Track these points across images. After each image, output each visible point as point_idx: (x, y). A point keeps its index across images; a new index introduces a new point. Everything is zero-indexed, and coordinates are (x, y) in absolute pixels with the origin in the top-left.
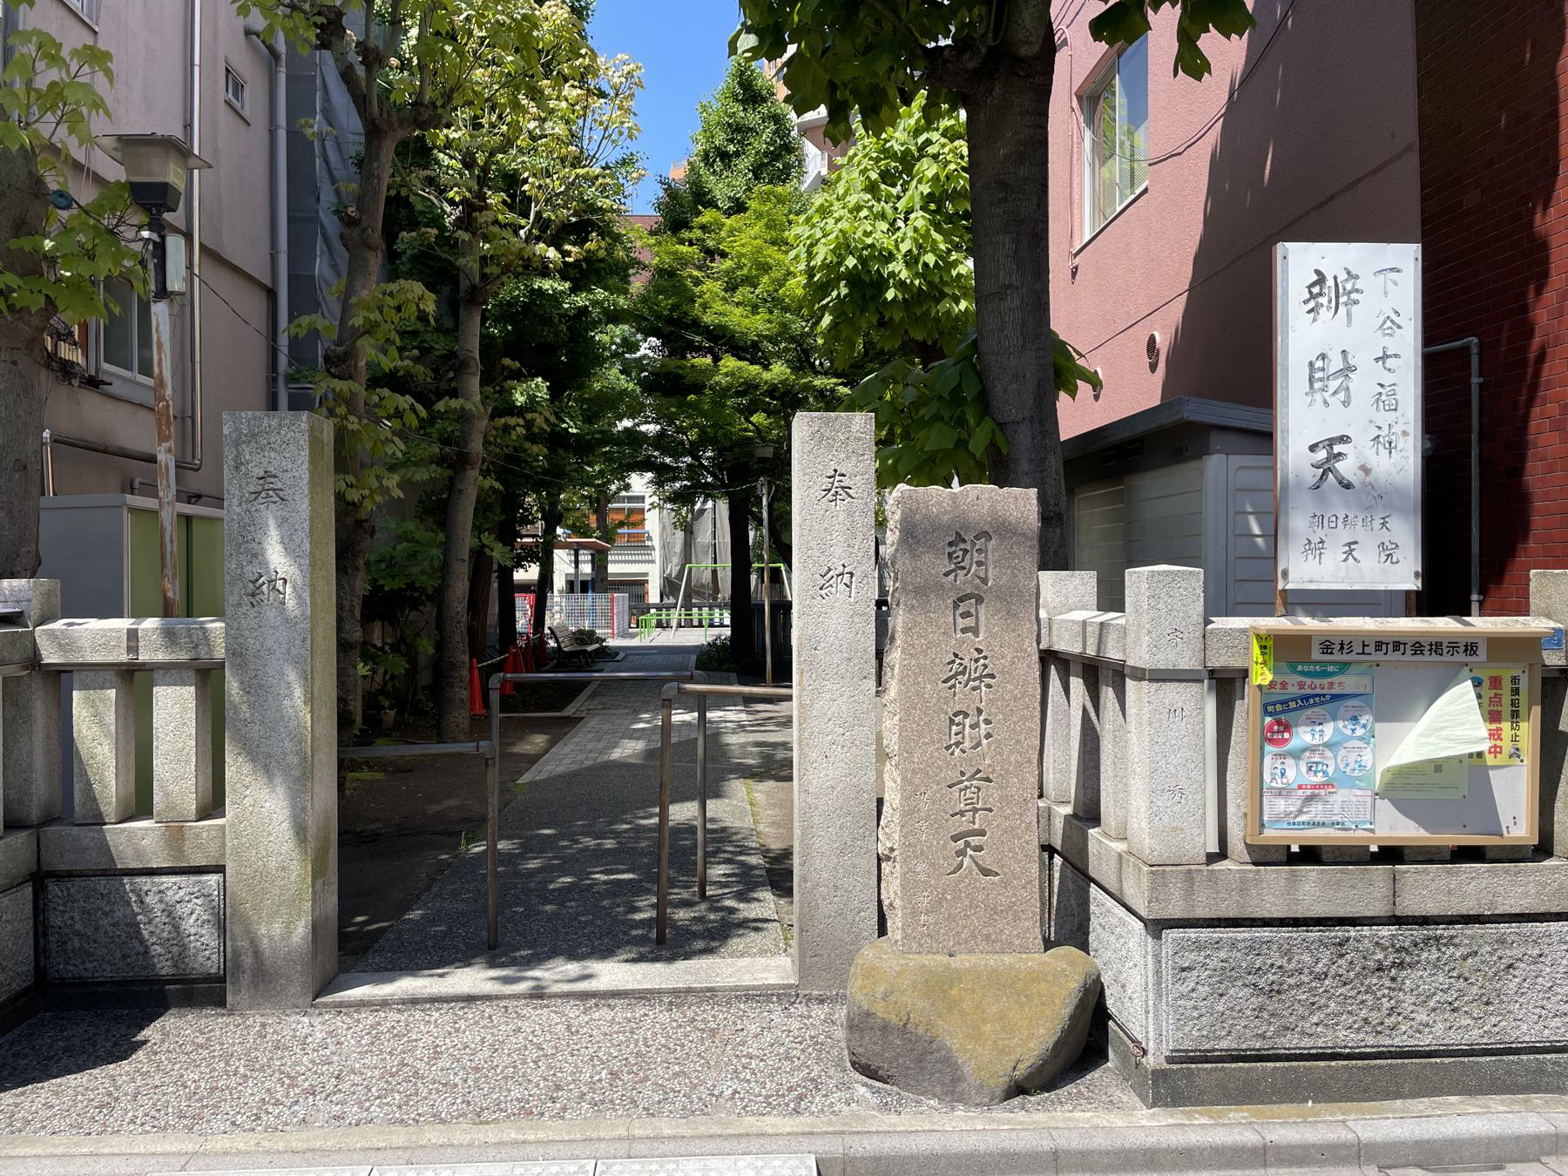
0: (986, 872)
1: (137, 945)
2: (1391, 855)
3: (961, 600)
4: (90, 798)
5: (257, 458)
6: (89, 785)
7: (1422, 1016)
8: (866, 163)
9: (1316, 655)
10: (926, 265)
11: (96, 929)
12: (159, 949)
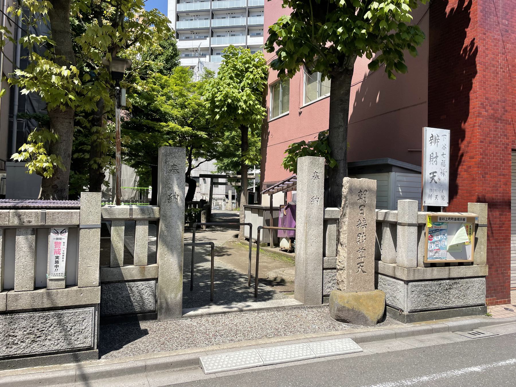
0: (364, 272)
1: (130, 303)
2: (447, 264)
3: (361, 206)
4: (116, 259)
5: (171, 160)
6: (115, 255)
7: (453, 300)
8: (230, 71)
9: (439, 221)
10: (250, 104)
11: (117, 299)
12: (136, 304)
